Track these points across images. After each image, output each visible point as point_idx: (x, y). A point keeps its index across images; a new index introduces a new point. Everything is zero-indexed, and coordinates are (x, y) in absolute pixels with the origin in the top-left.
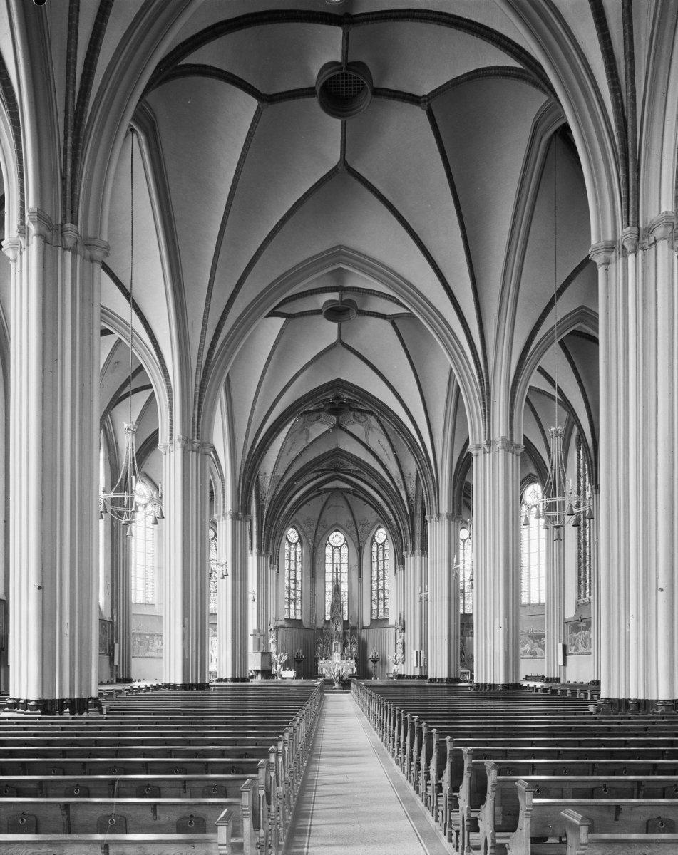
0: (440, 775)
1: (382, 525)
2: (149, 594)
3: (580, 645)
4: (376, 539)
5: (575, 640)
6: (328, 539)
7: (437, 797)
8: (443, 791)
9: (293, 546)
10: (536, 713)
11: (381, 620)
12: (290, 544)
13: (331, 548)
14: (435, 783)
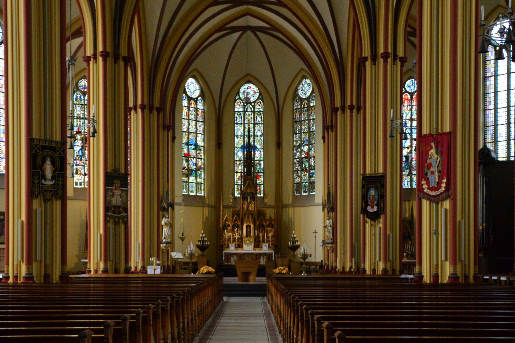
4: (300, 92)
6: (238, 93)
9: (192, 102)
12: (190, 99)
13: (242, 104)
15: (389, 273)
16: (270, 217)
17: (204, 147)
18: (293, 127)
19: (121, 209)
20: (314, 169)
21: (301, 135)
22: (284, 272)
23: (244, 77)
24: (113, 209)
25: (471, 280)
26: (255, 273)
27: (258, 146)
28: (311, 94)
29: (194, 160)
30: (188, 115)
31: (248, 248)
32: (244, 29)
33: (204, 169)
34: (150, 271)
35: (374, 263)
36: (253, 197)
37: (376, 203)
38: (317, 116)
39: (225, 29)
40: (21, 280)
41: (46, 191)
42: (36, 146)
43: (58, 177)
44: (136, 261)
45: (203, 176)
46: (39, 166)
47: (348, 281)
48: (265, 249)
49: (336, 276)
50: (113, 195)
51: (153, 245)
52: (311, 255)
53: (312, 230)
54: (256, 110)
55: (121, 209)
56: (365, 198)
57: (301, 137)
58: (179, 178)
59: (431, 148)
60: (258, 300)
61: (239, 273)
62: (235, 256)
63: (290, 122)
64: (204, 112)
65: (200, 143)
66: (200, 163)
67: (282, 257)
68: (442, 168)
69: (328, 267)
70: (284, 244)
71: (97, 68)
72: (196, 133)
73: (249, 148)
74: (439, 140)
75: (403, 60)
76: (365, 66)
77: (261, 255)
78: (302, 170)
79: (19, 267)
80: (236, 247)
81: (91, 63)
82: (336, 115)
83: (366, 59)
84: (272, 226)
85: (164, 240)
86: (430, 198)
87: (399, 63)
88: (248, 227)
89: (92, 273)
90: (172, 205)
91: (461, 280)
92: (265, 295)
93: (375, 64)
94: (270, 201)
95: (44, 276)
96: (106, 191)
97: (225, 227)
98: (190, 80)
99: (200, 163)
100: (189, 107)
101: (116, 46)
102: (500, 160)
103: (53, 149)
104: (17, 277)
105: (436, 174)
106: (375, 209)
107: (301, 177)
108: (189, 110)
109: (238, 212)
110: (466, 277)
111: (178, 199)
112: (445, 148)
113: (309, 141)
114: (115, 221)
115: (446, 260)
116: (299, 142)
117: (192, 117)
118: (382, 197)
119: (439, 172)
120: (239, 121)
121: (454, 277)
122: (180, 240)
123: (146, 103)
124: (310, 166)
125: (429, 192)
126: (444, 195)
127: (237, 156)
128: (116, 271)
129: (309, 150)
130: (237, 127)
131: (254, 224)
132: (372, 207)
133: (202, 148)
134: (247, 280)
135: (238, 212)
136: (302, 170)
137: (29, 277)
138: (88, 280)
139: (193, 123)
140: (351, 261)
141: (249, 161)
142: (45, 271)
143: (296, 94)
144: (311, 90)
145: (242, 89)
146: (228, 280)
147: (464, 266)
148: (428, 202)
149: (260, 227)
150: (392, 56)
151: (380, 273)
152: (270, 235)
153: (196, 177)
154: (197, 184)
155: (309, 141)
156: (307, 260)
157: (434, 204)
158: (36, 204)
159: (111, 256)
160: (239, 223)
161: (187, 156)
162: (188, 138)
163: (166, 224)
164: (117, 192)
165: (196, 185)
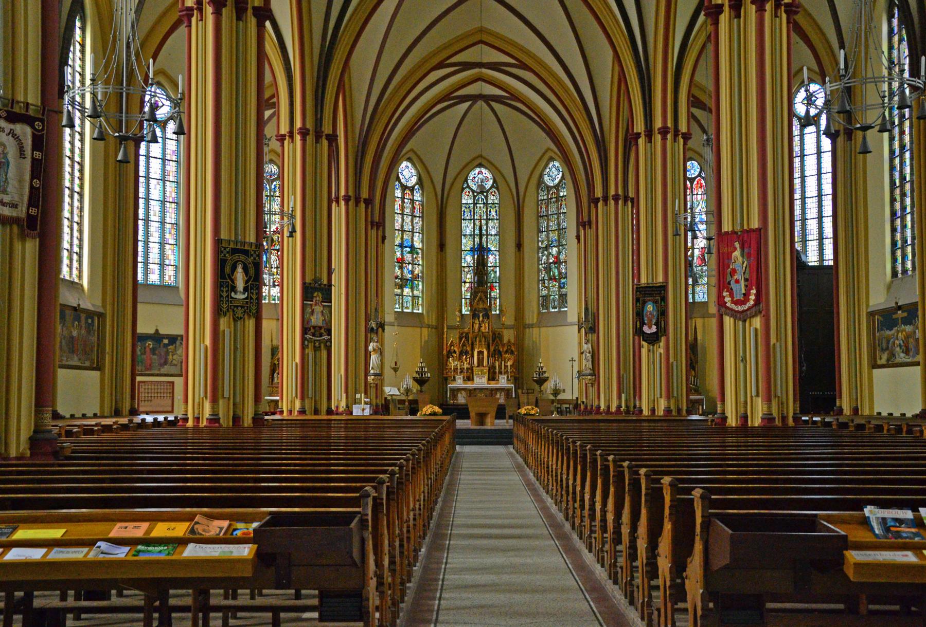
0: (679, 567)
1: (556, 157)
2: (170, 271)
3: (898, 349)
4: (546, 178)
5: (888, 342)
6: (466, 180)
7: (675, 611)
8: (689, 598)
9: (407, 191)
10: (338, 433)
11: (153, 286)
12: (404, 188)
13: (471, 194)
14: (668, 584)
15: (674, 413)
16: (509, 341)
17: (422, 249)
18: (538, 222)
19: (322, 331)
20: (566, 278)
21: (548, 234)
22: (533, 412)
23: (474, 159)
24: (312, 330)
25: (791, 422)
26: (494, 414)
27: (493, 249)
28: (561, 181)
29: (410, 267)
30: (402, 208)
31: (481, 381)
32: (474, 98)
33: (422, 278)
34: (357, 411)
35: (653, 400)
36: (487, 316)
37: (654, 321)
38: (569, 209)
39: (450, 98)
40: (204, 423)
41: (237, 307)
42: (225, 249)
43: (252, 289)
44: (339, 400)
45: (420, 287)
46: (229, 275)
47: (615, 425)
48: (503, 382)
49: (600, 417)
50: (312, 313)
51: (362, 380)
52: (564, 391)
53: (563, 358)
54: (490, 202)
55: (322, 331)
56: (639, 315)
57: (548, 236)
58: (390, 289)
59: (735, 249)
60: (500, 449)
61: (472, 414)
62: (463, 392)
63: (534, 218)
64: (422, 205)
65: (418, 245)
66: (417, 270)
67: (528, 393)
68: (751, 277)
69: (586, 407)
70: (528, 378)
71: (294, 149)
72: (412, 232)
73: (481, 251)
74: (745, 239)
75: (687, 137)
76: (637, 145)
77: (497, 390)
78: (550, 279)
79: (201, 406)
80: (464, 380)
81: (286, 142)
82: (596, 207)
83: (638, 135)
84: (512, 353)
85: (372, 372)
86: (734, 314)
87: (681, 141)
88: (480, 353)
89: (285, 414)
90: (382, 326)
91: (778, 423)
92: (511, 443)
93: (650, 141)
94: (508, 319)
95: (233, 418)
96: (303, 308)
97: (450, 353)
98: (404, 164)
99: (417, 270)
100: (403, 199)
101: (318, 122)
102: (810, 264)
103: (246, 253)
104: (198, 418)
105: (743, 282)
106: (654, 329)
107: (548, 288)
108: (403, 202)
109: (467, 334)
110: (784, 418)
111: (389, 318)
112: (753, 251)
113: (559, 241)
114: (315, 347)
115: (758, 395)
116: (546, 242)
117: (407, 211)
118: (663, 313)
119: (746, 280)
120: (467, 215)
121: (768, 418)
122: (392, 371)
123: (351, 193)
124: (560, 273)
125: (733, 306)
126: (754, 310)
127: (465, 261)
128: (316, 412)
129: (559, 253)
130: (464, 223)
131: (488, 349)
132: (650, 327)
133: (420, 251)
134: (482, 423)
135: (467, 334)
136: (550, 279)
137: (214, 420)
138: (281, 423)
139: (408, 220)
140: (619, 398)
141: (481, 267)
142: (234, 412)
143: (540, 181)
144: (560, 176)
145: (471, 175)
146: (461, 424)
147: (781, 404)
148: (732, 320)
149: (496, 354)
150: (672, 131)
151: (661, 413)
152: (509, 364)
153: (412, 289)
154: (414, 297)
155: (559, 241)
156: (559, 397)
157: (741, 323)
158: (224, 322)
159: (310, 392)
160: (469, 349)
161: (401, 261)
162: (402, 238)
163: (374, 350)
164: (318, 309)
165: (413, 299)
